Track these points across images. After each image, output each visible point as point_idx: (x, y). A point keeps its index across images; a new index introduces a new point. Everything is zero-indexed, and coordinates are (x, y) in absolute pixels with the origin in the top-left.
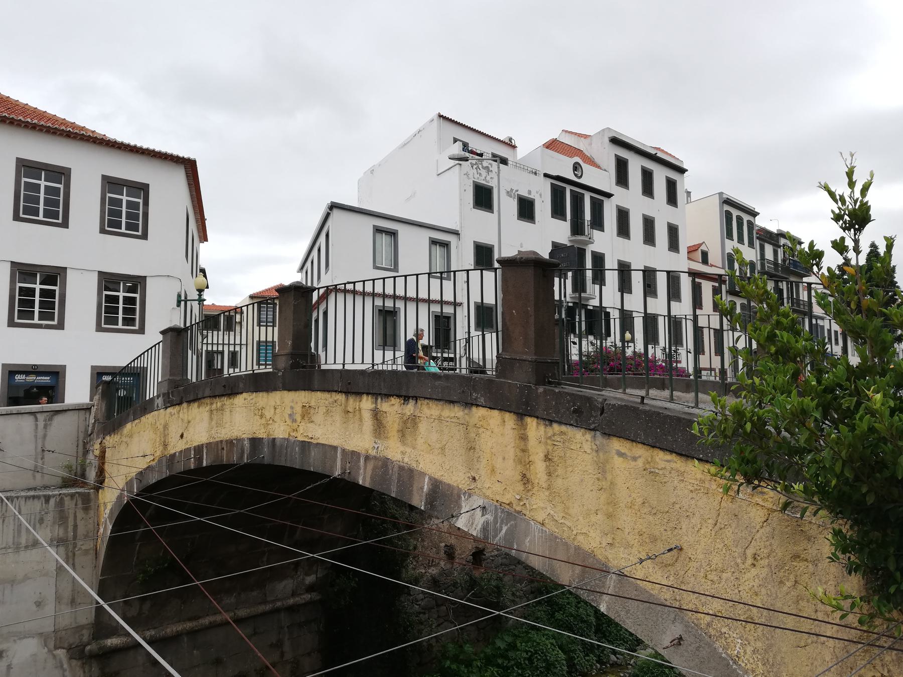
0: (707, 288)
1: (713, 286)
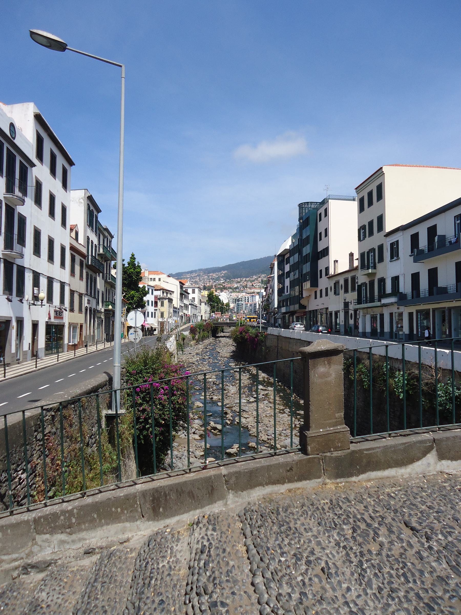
0: (78, 258)
1: (80, 259)
